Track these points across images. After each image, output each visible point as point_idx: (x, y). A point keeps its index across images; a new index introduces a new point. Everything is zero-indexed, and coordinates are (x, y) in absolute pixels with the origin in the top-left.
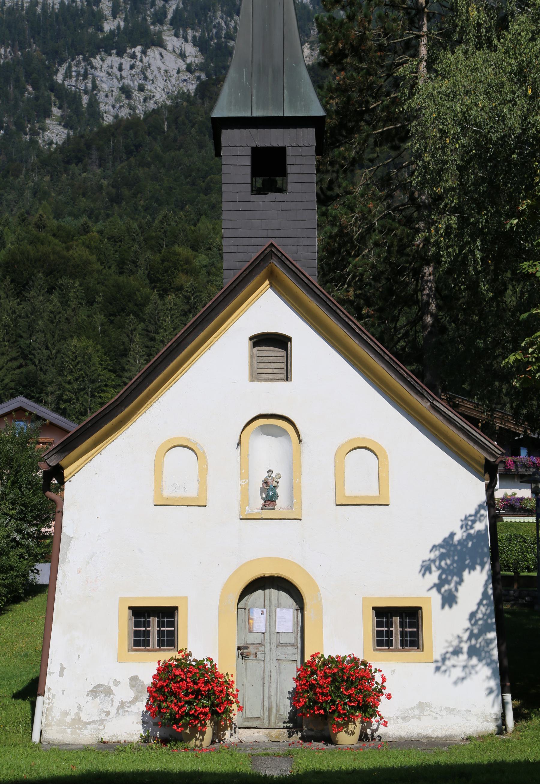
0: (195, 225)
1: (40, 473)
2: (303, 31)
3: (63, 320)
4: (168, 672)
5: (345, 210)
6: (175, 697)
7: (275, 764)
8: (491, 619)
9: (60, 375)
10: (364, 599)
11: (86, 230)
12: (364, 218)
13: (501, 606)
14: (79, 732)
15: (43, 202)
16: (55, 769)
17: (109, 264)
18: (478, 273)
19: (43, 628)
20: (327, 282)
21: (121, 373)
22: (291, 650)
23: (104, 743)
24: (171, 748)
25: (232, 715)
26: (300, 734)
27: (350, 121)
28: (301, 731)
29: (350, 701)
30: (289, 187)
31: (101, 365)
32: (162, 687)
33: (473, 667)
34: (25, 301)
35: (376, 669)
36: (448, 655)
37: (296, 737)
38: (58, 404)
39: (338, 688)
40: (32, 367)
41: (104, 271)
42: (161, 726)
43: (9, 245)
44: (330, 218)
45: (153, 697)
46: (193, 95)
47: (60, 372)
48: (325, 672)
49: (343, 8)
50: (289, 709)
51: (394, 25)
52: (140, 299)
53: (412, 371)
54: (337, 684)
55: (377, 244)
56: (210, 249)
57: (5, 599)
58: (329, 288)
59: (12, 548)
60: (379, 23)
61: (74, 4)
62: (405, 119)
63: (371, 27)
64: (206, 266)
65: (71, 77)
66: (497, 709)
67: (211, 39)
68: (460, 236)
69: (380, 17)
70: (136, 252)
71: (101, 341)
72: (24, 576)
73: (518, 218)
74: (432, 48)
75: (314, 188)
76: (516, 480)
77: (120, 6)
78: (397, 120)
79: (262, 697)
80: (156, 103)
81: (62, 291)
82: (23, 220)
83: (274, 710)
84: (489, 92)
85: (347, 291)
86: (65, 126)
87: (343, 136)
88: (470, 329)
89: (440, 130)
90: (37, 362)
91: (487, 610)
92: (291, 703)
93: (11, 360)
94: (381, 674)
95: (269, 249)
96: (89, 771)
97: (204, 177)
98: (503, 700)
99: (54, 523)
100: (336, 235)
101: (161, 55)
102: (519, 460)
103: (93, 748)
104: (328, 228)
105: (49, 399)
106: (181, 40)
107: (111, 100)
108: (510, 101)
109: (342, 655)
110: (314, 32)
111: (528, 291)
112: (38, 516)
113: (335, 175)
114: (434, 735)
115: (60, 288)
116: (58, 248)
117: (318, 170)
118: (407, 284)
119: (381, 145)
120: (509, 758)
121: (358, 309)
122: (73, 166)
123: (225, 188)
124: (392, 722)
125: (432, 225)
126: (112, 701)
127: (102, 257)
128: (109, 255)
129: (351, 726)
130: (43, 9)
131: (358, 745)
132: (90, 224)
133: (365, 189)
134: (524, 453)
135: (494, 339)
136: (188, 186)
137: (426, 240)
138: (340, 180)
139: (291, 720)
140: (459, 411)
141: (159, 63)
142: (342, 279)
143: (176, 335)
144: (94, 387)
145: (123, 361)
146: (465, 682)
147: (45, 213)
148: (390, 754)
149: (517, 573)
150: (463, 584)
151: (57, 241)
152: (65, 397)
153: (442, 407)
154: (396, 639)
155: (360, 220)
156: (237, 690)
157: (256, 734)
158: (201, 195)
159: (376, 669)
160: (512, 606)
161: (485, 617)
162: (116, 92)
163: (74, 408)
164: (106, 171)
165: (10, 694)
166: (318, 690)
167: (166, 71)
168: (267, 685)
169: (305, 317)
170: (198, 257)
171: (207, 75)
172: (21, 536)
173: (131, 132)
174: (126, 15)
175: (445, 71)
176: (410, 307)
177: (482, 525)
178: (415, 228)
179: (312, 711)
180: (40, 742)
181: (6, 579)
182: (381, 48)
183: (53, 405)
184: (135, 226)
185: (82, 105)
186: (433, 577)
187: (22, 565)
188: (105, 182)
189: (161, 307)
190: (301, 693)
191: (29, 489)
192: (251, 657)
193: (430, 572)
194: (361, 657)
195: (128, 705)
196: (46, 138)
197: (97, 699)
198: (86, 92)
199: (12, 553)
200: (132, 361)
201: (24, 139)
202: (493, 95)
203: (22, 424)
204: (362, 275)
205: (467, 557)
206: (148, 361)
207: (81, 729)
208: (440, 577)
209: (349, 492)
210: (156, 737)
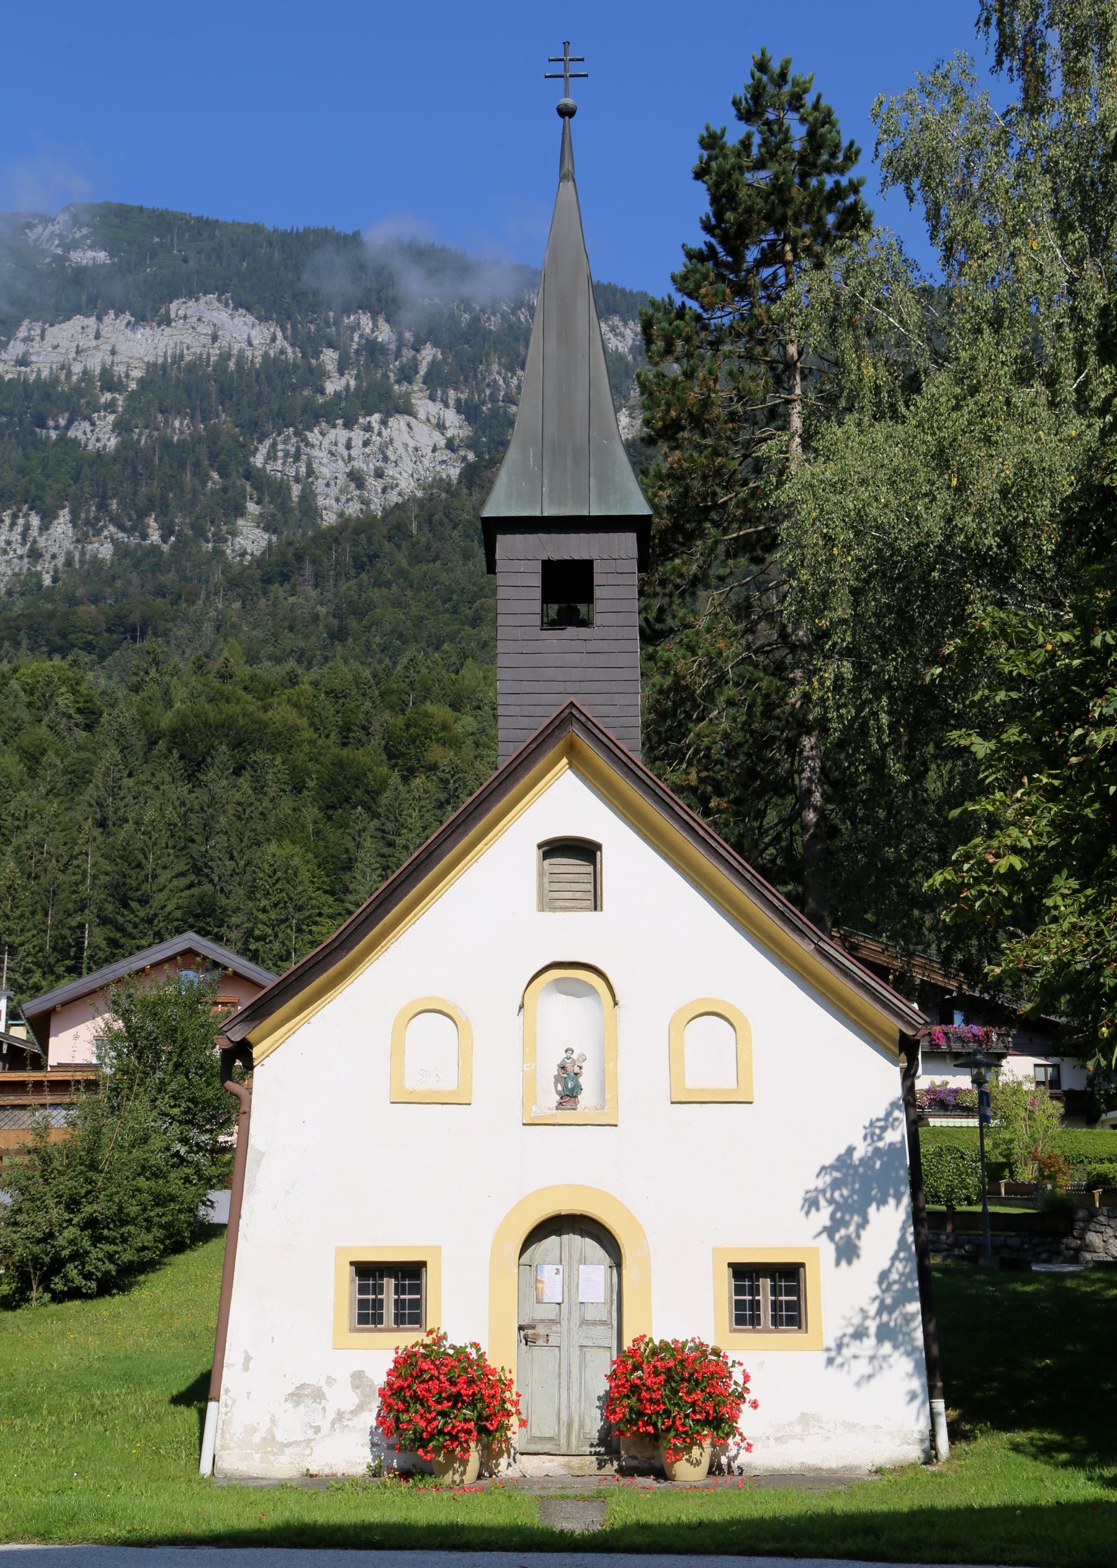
0: (457, 673)
1: (217, 1052)
2: (617, 390)
3: (256, 815)
4: (411, 1364)
5: (682, 651)
6: (422, 1405)
7: (577, 1513)
8: (913, 1282)
9: (250, 898)
10: (715, 1250)
11: (293, 680)
12: (711, 664)
13: (927, 1262)
14: (273, 1458)
15: (229, 639)
16: (235, 1517)
17: (326, 732)
18: (884, 747)
19: (218, 1292)
20: (656, 759)
21: (342, 896)
22: (601, 1330)
23: (312, 1476)
24: (415, 1485)
25: (509, 1434)
26: (616, 1463)
27: (688, 521)
28: (619, 1459)
29: (694, 1412)
30: (598, 619)
31: (313, 883)
32: (401, 1388)
33: (885, 1358)
34: (200, 786)
35: (734, 1362)
36: (846, 1340)
37: (611, 1468)
38: (246, 942)
39: (675, 1392)
40: (208, 888)
41: (320, 742)
42: (400, 1450)
43: (178, 705)
44: (660, 664)
45: (387, 1405)
46: (455, 482)
47: (251, 895)
48: (654, 1366)
49: (677, 360)
50: (599, 1424)
51: (752, 385)
52: (372, 783)
53: (787, 895)
54: (673, 1384)
55: (730, 703)
56: (479, 708)
57: (162, 1247)
58: (659, 768)
59: (173, 1166)
60: (730, 383)
61: (283, 357)
62: (771, 519)
63: (718, 387)
64: (473, 734)
65: (275, 459)
66: (923, 1424)
67: (484, 403)
68: (856, 691)
69: (731, 374)
70: (368, 713)
71: (312, 846)
72: (190, 1210)
73: (943, 666)
74: (808, 418)
75: (636, 620)
76: (948, 1061)
77: (350, 359)
78: (759, 520)
79: (557, 1405)
80: (400, 494)
81: (256, 771)
82: (200, 667)
83: (576, 1427)
84: (895, 482)
85: (687, 773)
86: (266, 529)
87: (678, 542)
88: (873, 831)
89: (825, 536)
90: (217, 879)
91: (905, 1267)
92: (602, 1414)
93: (177, 876)
94: (742, 1368)
95: (567, 711)
96: (287, 1522)
97: (471, 602)
98: (931, 1409)
99: (236, 1127)
100: (670, 689)
101: (409, 425)
102: (952, 1030)
103: (294, 1484)
104: (657, 678)
105: (234, 935)
106: (440, 405)
107: (334, 491)
108: (926, 495)
109: (682, 1339)
110: (635, 393)
111: (959, 773)
112: (214, 1117)
113: (667, 600)
114: (826, 1465)
115: (252, 767)
116: (251, 708)
117: (641, 593)
118: (778, 763)
119: (735, 556)
120: (942, 1502)
121: (704, 800)
122: (275, 588)
123: (501, 620)
124: (759, 1445)
125: (814, 674)
126: (324, 1409)
127: (316, 720)
128: (327, 718)
129: (696, 1451)
130: (238, 364)
131: (707, 1481)
132: (299, 671)
133: (712, 621)
134: (958, 1018)
135: (910, 846)
136: (447, 615)
137: (806, 697)
138: (674, 607)
139: (602, 1441)
140: (860, 955)
141: (406, 438)
142: (677, 756)
143: (427, 838)
144: (301, 917)
145: (346, 877)
146: (873, 1381)
147: (232, 656)
148: (756, 1498)
149: (951, 1208)
150: (869, 1227)
151: (249, 697)
152: (257, 932)
153: (832, 952)
154: (766, 1313)
155: (705, 666)
156: (518, 1395)
157: (548, 1464)
158: (467, 627)
159: (734, 1362)
160: (944, 1259)
161: (903, 1279)
162: (342, 479)
163: (271, 949)
164: (325, 594)
165: (167, 1397)
166: (644, 1394)
167: (416, 449)
168: (564, 1385)
169: (622, 813)
170: (460, 719)
171: (478, 455)
172: (187, 1148)
173: (363, 536)
174: (358, 371)
175: (829, 450)
176: (782, 797)
177: (897, 1134)
178: (788, 679)
179: (635, 1428)
180: (213, 1474)
181: (163, 1215)
182: (733, 417)
183: (239, 944)
184: (367, 673)
185: (291, 498)
186: (823, 1216)
187: (188, 1194)
188: (322, 610)
189: (404, 795)
190: (618, 1399)
191: (201, 1076)
192: (540, 1342)
193: (818, 1209)
194: (711, 1342)
195: (349, 1417)
196: (237, 547)
197: (301, 1407)
198: (297, 480)
199: (172, 1175)
200: (359, 877)
201: (204, 549)
202: (902, 485)
203: (191, 974)
204: (709, 749)
205: (875, 1185)
206: (384, 878)
207: (276, 1454)
208: (833, 1216)
209: (690, 1084)
210: (392, 1468)
